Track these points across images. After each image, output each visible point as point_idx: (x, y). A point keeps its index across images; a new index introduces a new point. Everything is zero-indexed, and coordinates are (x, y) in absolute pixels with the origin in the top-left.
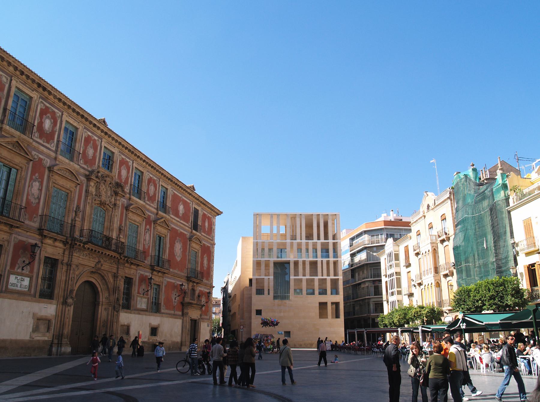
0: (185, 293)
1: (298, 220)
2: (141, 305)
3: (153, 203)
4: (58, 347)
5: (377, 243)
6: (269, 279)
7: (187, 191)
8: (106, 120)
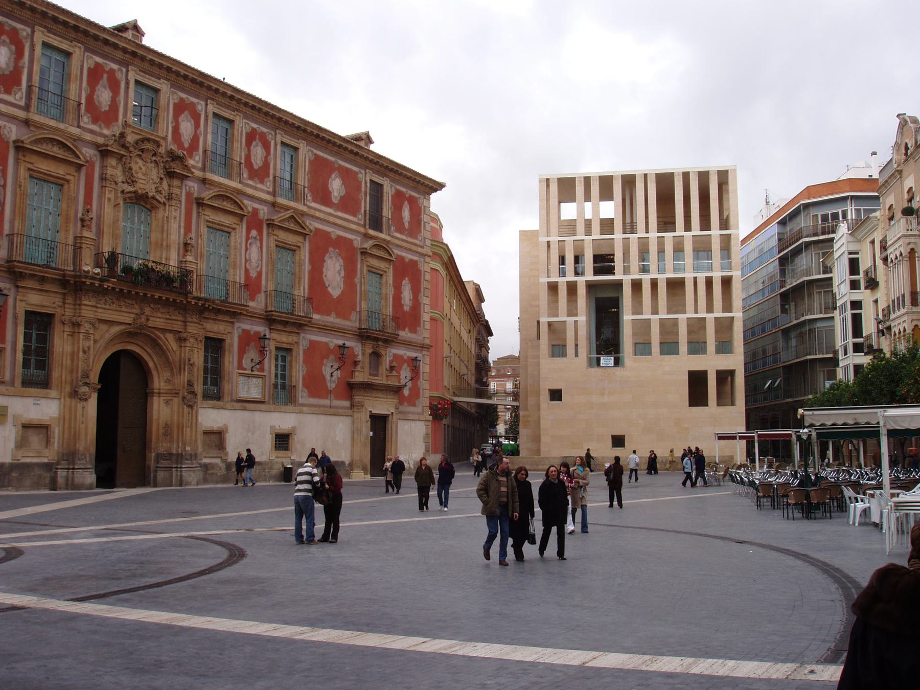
1: (640, 186)
3: (262, 182)
6: (580, 321)
8: (140, 24)
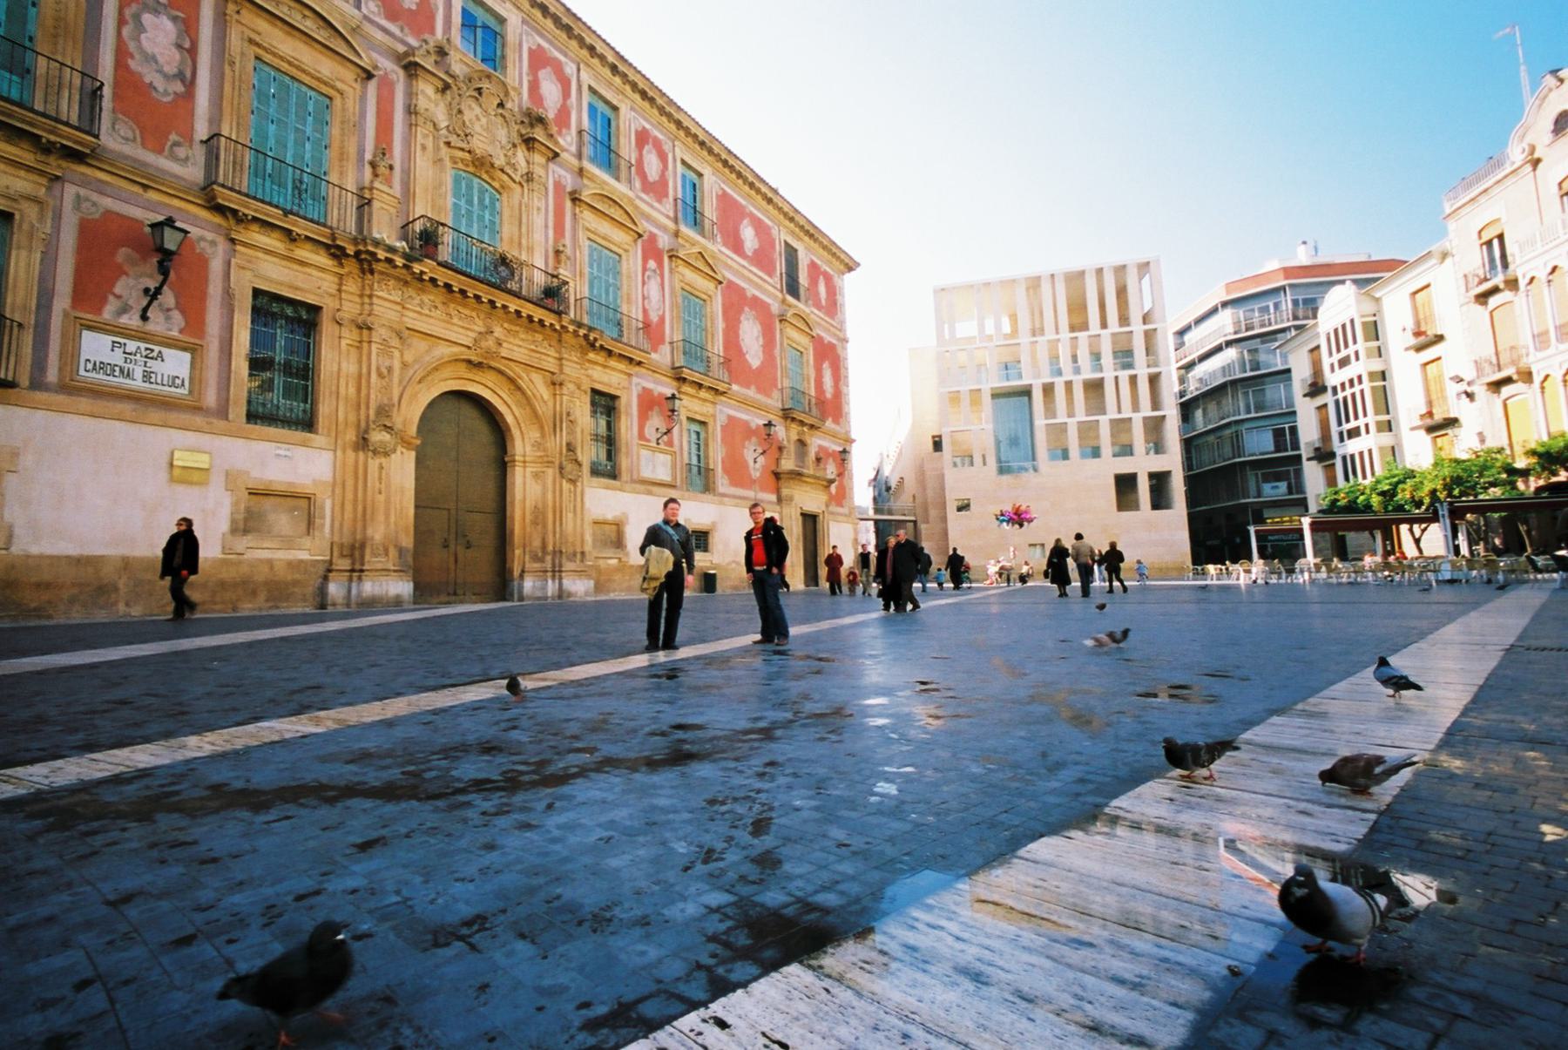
0: (780, 449)
1: (1046, 288)
2: (653, 471)
3: (660, 201)
4: (350, 580)
5: (1263, 326)
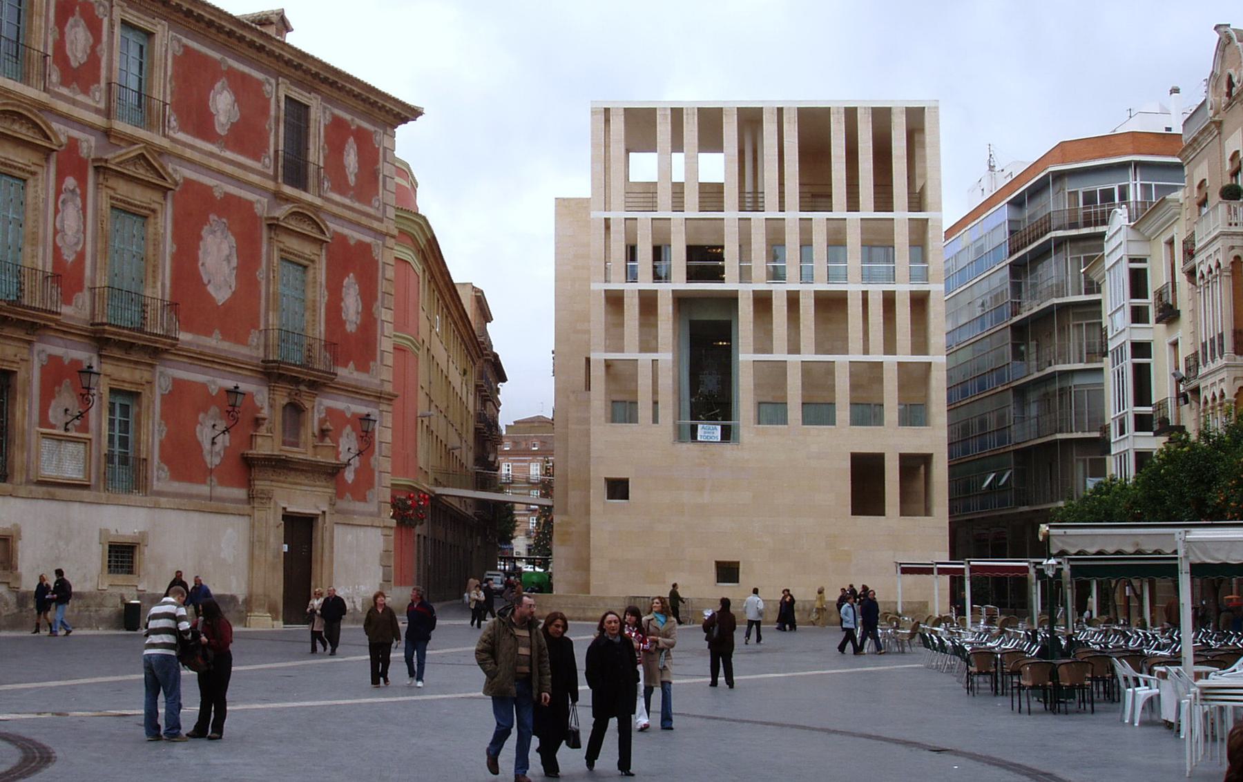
0: (257, 422)
1: (769, 128)
3: (86, 91)
6: (662, 361)
7: (241, 39)
